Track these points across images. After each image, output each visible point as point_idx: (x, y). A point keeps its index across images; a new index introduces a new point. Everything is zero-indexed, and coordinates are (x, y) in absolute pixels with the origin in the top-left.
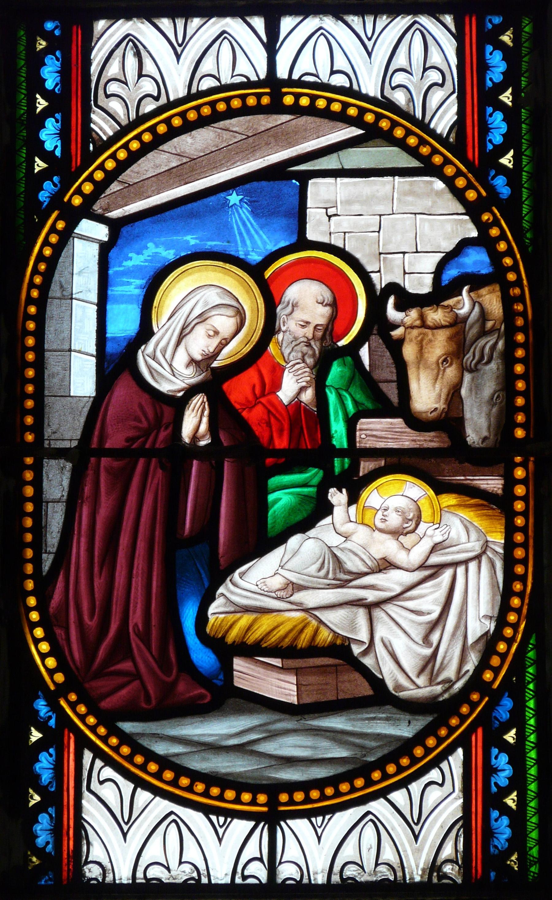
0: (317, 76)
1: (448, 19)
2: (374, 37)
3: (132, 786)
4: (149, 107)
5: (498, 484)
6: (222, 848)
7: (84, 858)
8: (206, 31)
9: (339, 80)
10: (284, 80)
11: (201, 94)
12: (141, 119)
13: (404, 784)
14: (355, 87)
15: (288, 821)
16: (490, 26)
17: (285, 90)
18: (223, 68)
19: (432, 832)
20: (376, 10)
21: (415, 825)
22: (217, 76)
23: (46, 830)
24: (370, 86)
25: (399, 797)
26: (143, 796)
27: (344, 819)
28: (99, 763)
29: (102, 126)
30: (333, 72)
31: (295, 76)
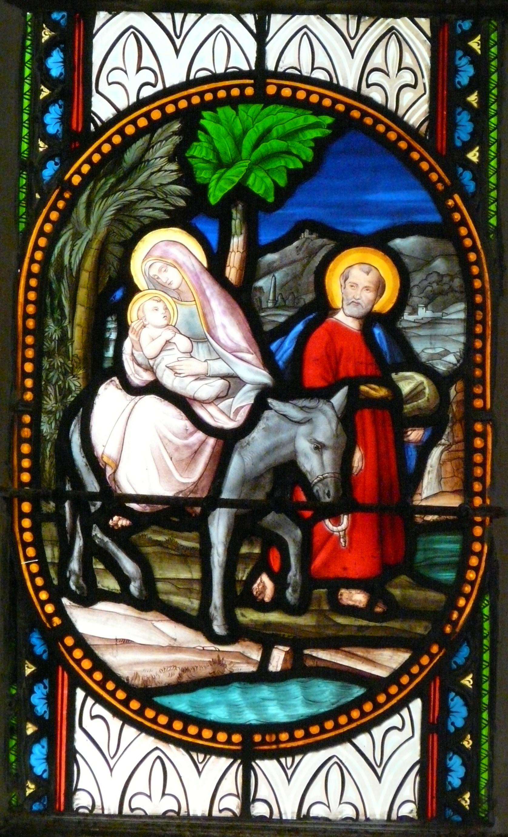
1: (424, 23)
2: (359, 36)
3: (121, 723)
4: (148, 91)
6: (202, 785)
7: (74, 785)
10: (271, 72)
12: (140, 103)
13: (366, 728)
14: (335, 81)
16: (459, 31)
18: (214, 60)
21: (377, 769)
23: (39, 759)
24: (349, 81)
25: (362, 740)
26: (130, 732)
27: (312, 760)
28: (90, 701)
29: (102, 110)
30: (313, 69)
31: (280, 70)
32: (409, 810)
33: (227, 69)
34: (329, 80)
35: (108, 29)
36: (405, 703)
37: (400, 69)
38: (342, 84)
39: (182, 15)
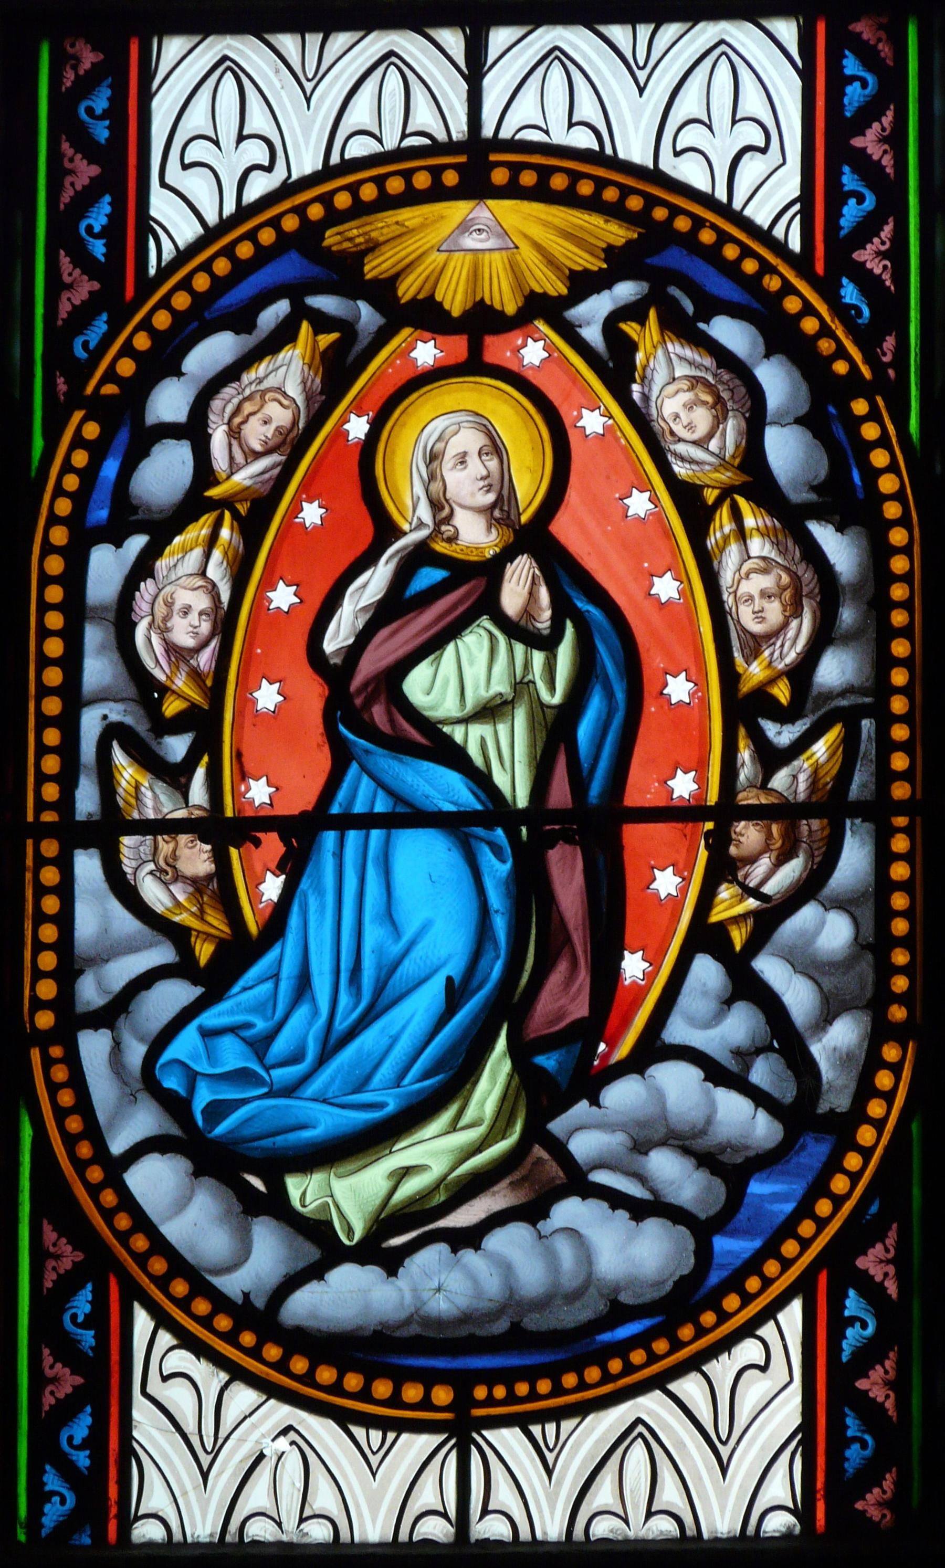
0: (547, 132)
5: (339, 855)
6: (380, 1483)
8: (743, 45)
9: (583, 140)
11: (350, 166)
12: (244, 212)
13: (695, 1364)
14: (609, 151)
15: (484, 1433)
17: (493, 157)
19: (748, 1460)
20: (328, 26)
22: (379, 135)
24: (634, 147)
25: (690, 1387)
26: (243, 1397)
28: (165, 1339)
31: (505, 134)
32: (778, 1523)
33: (404, 136)
34: (597, 148)
35: (182, 63)
36: (770, 1312)
37: (734, 122)
38: (621, 155)
39: (320, 36)
